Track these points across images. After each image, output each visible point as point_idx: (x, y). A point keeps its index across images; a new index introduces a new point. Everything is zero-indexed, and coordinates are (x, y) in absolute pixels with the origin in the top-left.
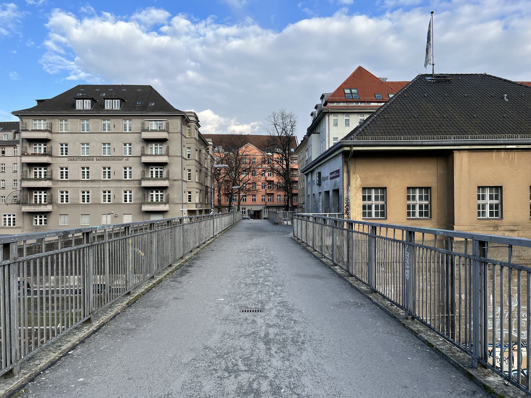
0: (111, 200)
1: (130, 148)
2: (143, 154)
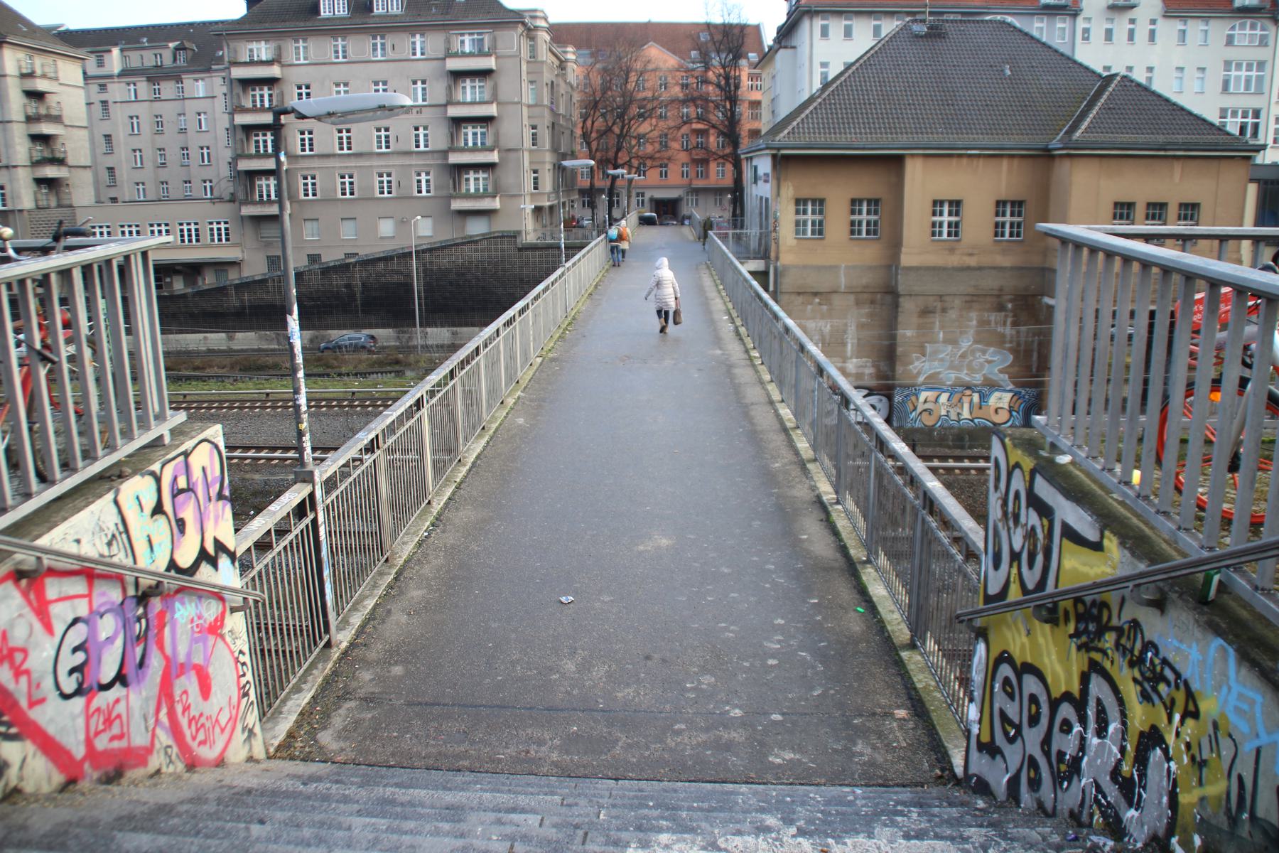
0: (394, 190)
1: (424, 89)
2: (450, 102)
